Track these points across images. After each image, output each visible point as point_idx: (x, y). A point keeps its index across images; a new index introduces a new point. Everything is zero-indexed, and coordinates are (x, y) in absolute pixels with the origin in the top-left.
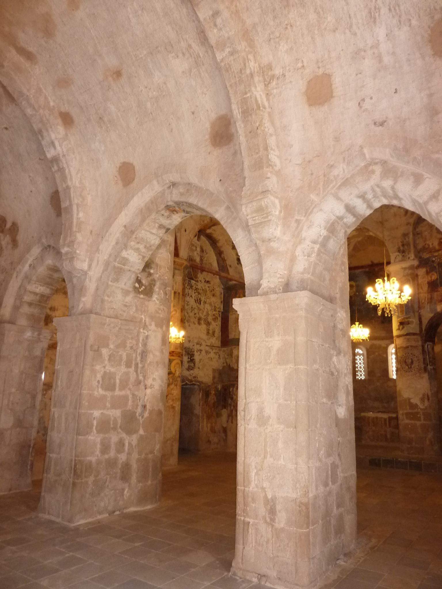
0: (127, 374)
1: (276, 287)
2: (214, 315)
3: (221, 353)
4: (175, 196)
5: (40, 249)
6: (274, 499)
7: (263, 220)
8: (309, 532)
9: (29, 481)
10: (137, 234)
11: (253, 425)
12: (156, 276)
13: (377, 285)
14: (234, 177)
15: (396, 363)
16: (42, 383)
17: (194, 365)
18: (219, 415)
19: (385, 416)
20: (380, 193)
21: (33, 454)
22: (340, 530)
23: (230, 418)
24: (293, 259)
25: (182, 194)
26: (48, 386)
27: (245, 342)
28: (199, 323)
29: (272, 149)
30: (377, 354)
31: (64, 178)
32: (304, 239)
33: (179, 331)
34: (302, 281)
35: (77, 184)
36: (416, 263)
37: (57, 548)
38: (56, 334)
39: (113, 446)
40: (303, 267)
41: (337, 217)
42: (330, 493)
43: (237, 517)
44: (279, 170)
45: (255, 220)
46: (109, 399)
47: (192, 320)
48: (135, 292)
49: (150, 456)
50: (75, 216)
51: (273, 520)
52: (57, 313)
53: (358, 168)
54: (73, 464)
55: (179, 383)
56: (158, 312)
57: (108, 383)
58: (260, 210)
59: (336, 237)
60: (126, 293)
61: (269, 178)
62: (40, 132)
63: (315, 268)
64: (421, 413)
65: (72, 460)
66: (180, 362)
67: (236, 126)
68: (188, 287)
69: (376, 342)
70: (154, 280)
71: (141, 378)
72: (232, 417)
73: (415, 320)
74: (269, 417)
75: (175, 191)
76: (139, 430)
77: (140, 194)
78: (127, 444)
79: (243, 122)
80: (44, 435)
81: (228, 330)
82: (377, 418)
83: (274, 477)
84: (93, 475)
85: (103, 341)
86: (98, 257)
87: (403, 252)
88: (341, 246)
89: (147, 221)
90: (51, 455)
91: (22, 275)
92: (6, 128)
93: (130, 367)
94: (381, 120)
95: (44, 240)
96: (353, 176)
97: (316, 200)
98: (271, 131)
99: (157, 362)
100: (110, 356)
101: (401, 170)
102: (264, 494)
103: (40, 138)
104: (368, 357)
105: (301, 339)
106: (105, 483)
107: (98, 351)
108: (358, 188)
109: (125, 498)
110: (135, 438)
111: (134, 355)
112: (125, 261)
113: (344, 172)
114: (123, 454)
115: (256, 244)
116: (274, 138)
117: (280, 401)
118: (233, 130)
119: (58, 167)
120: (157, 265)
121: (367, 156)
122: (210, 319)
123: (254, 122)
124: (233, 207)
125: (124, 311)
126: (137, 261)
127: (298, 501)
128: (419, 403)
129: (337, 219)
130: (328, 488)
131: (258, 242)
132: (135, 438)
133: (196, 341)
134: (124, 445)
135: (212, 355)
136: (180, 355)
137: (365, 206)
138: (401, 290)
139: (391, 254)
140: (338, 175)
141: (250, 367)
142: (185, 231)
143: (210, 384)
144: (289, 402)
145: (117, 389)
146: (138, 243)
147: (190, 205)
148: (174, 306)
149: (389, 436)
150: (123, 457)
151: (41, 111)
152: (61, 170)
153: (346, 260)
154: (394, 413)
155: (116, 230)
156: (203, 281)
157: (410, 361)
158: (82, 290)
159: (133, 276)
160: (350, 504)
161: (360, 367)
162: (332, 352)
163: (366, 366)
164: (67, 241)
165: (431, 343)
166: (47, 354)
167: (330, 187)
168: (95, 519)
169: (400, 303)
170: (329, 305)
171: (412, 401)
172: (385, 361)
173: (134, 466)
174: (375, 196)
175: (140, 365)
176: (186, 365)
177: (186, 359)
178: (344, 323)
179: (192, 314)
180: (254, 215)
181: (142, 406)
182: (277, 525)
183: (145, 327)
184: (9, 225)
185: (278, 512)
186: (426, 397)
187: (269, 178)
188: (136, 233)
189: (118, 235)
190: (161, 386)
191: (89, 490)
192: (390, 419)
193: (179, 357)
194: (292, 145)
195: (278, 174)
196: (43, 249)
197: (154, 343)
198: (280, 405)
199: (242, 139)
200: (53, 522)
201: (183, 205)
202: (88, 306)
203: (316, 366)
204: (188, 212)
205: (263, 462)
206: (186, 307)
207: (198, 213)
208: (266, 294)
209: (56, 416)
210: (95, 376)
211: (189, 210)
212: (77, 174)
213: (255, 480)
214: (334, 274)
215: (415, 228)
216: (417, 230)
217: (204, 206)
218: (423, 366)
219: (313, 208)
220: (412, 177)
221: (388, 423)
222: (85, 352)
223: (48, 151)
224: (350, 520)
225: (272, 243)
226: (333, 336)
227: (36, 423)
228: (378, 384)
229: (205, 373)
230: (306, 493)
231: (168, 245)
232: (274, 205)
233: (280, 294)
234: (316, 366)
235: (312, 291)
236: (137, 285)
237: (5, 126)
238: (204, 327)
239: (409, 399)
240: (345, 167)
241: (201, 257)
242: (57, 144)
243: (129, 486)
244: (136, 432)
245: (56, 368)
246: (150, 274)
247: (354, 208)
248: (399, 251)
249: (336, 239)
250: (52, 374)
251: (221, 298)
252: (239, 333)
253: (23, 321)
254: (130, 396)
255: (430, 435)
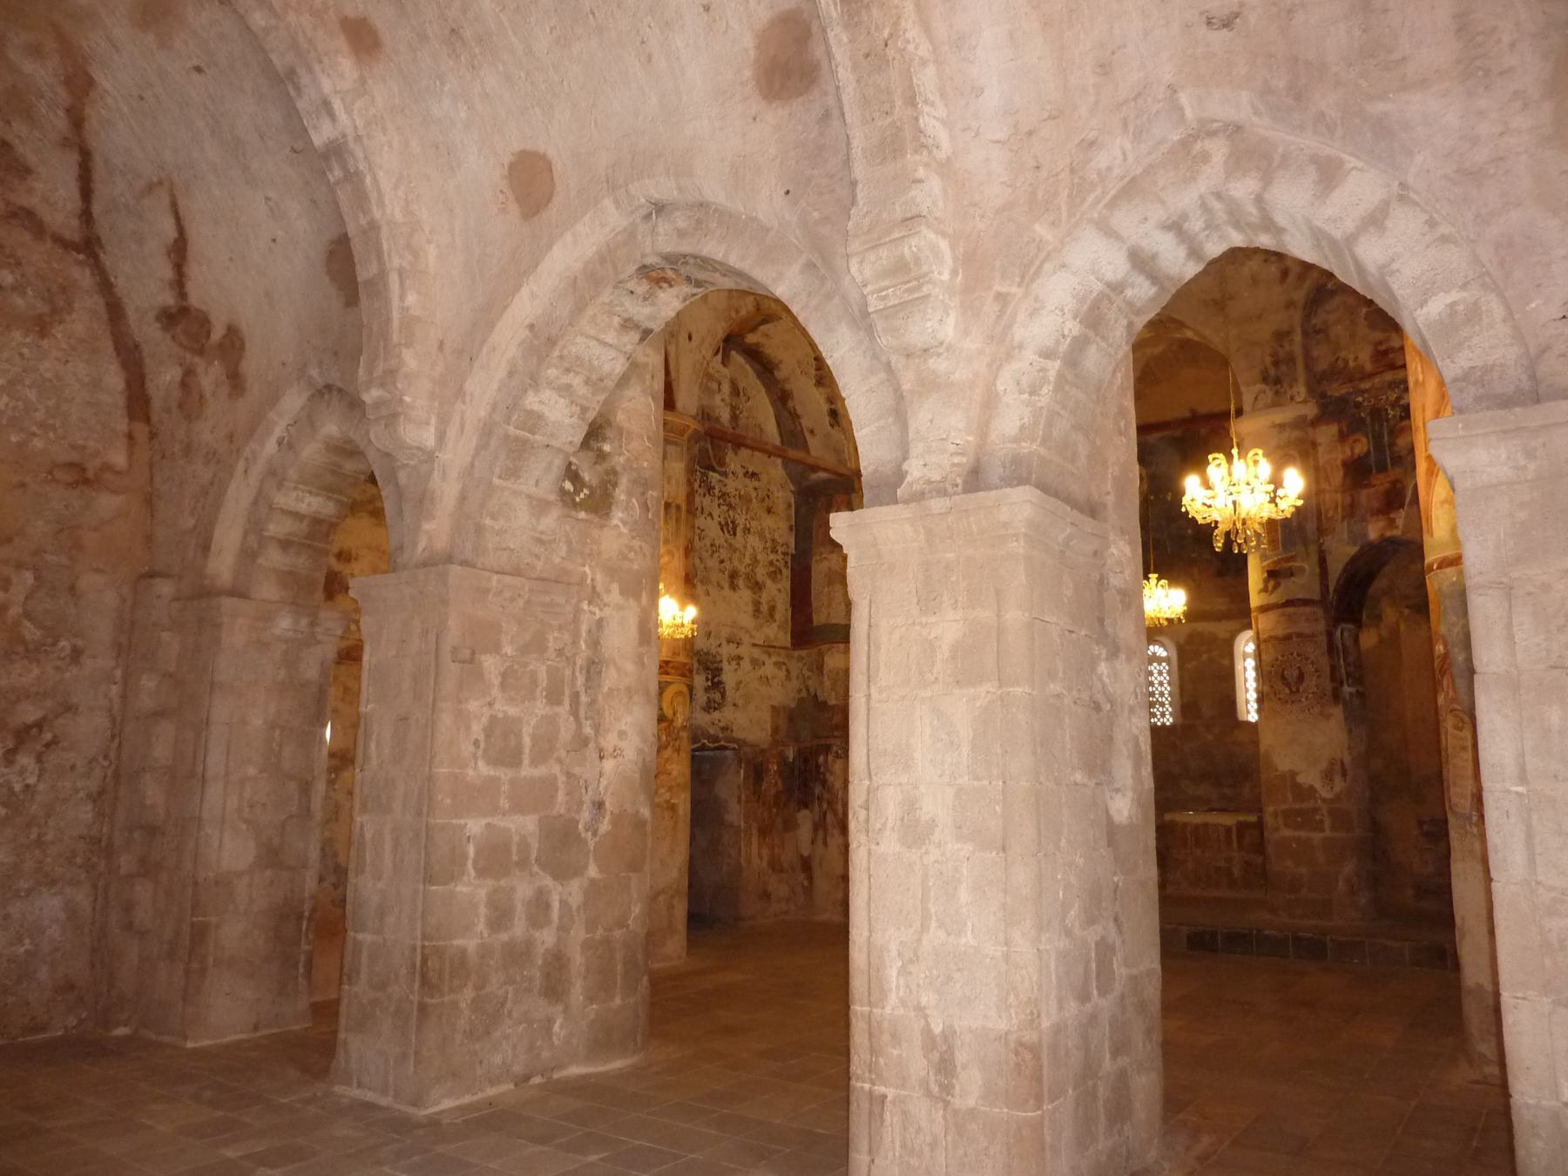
0: (551, 720)
1: (944, 479)
2: (771, 563)
3: (795, 666)
4: (664, 240)
5: (306, 395)
6: (949, 1035)
7: (907, 297)
8: (1042, 1117)
9: (303, 1004)
10: (564, 347)
11: (890, 845)
12: (619, 461)
13: (1212, 470)
14: (823, 179)
15: (1257, 680)
16: (325, 752)
17: (723, 696)
18: (790, 825)
19: (1229, 820)
20: (1224, 217)
21: (311, 936)
22: (1120, 1111)
23: (821, 833)
24: (990, 402)
25: (682, 234)
26: (343, 759)
27: (866, 627)
28: (734, 587)
29: (926, 102)
30: (1205, 657)
31: (361, 198)
32: (1021, 346)
33: (683, 607)
34: (1017, 460)
35: (399, 217)
36: (1311, 410)
37: (386, 1169)
38: (357, 622)
39: (520, 910)
40: (1018, 424)
41: (1109, 285)
42: (1093, 1018)
43: (853, 1082)
44: (948, 159)
45: (886, 297)
46: (505, 788)
47: (714, 577)
48: (565, 504)
49: (618, 934)
50: (395, 303)
51: (947, 1089)
52: (355, 567)
53: (1164, 148)
54: (419, 959)
55: (686, 746)
56: (625, 558)
57: (503, 745)
58: (900, 268)
59: (1103, 338)
60: (540, 507)
61: (920, 181)
62: (291, 73)
63: (1049, 425)
64: (1325, 811)
65: (414, 949)
66: (685, 689)
67: (826, 40)
68: (701, 491)
69: (1202, 626)
70: (614, 472)
71: (588, 730)
72: (826, 830)
73: (1309, 566)
74: (932, 824)
75: (663, 226)
76: (586, 867)
77: (568, 237)
78: (556, 905)
79: (846, 26)
80: (335, 886)
81: (809, 604)
82: (1206, 825)
83: (950, 978)
84: (470, 985)
85: (484, 636)
86: (463, 412)
87: (1277, 381)
88: (1117, 366)
89: (590, 312)
90: (360, 937)
91: (258, 469)
92: (198, 69)
93: (559, 703)
94: (1226, 11)
95: (314, 372)
96: (1150, 170)
97: (1050, 237)
98: (924, 50)
99: (628, 689)
100: (504, 675)
101: (1280, 150)
102: (923, 1022)
103: (292, 93)
104: (1181, 667)
105: (1015, 616)
106: (503, 1004)
107: (471, 661)
108: (1163, 203)
109: (556, 1042)
110: (574, 891)
111: (568, 672)
112: (534, 421)
113: (1125, 160)
114: (546, 931)
115: (889, 364)
116: (931, 70)
117: (960, 781)
118: (819, 52)
119: (344, 168)
120: (620, 431)
121: (1189, 114)
122: (761, 573)
123: (877, 27)
124: (823, 264)
125: (537, 557)
126: (568, 421)
127: (1013, 1037)
128: (1318, 785)
129: (1107, 291)
130: (1089, 1007)
131: (894, 359)
132: (574, 891)
133: (725, 632)
134: (548, 906)
135: (769, 669)
136: (686, 672)
137: (1181, 252)
138: (1277, 482)
139: (1243, 389)
140: (1109, 169)
141: (880, 692)
142: (690, 338)
143: (765, 746)
144: (986, 783)
145: (526, 762)
146: (568, 370)
147: (705, 263)
148: (666, 542)
149: (1237, 872)
150: (546, 938)
151: (291, 17)
152: (353, 178)
153: (1129, 403)
154: (1250, 811)
155: (508, 336)
156: (740, 473)
157: (1295, 673)
158: (424, 502)
159: (558, 463)
160: (1145, 1047)
161: (1162, 694)
162: (1096, 650)
163: (1177, 691)
164: (378, 373)
165: (1351, 626)
166: (335, 678)
167: (1086, 205)
168: (480, 1096)
169: (1274, 516)
170: (1088, 523)
171: (1300, 779)
172: (1227, 677)
173: (577, 959)
174: (1210, 226)
175: (584, 699)
176: (701, 698)
177: (700, 681)
178: (1127, 572)
179: (712, 563)
180: (885, 283)
181: (593, 803)
182: (957, 1102)
183: (594, 596)
184: (217, 334)
185: (959, 1069)
186: (1338, 767)
187: (920, 181)
188: (561, 343)
189: (513, 351)
190: (640, 751)
191: (462, 1023)
192: (1242, 827)
193: (683, 675)
194: (982, 90)
195: (945, 168)
196: (313, 396)
197: (620, 639)
198: (960, 791)
199: (845, 75)
200: (371, 1106)
201: (686, 263)
202: (441, 544)
203: (1055, 687)
204: (698, 284)
205: (919, 940)
206: (697, 544)
207: (728, 283)
208: (918, 497)
209: (368, 836)
210: (468, 728)
211: (701, 276)
212: (396, 187)
213: (898, 987)
214: (1098, 443)
215: (1307, 317)
216: (1314, 321)
217: (745, 266)
218: (1328, 685)
219: (1042, 262)
220: (1311, 169)
221: (1234, 836)
222: (437, 665)
223: (315, 127)
224: (1146, 1086)
225: (931, 361)
226: (1100, 610)
227: (314, 854)
228: (1210, 737)
229: (750, 718)
230: (1033, 1020)
231: (648, 376)
232: (937, 254)
233: (957, 498)
234: (1055, 687)
235: (1043, 487)
236: (568, 486)
237: (195, 62)
238: (745, 595)
239: (1293, 774)
240: (1128, 146)
241: (733, 408)
242: (337, 105)
243: (566, 1011)
244: (578, 871)
245: (362, 709)
246: (602, 456)
247: (1154, 257)
248: (1265, 379)
249: (1104, 344)
250: (353, 726)
251: (789, 518)
252: (848, 605)
253: (269, 591)
254: (562, 779)
255: (1349, 867)
